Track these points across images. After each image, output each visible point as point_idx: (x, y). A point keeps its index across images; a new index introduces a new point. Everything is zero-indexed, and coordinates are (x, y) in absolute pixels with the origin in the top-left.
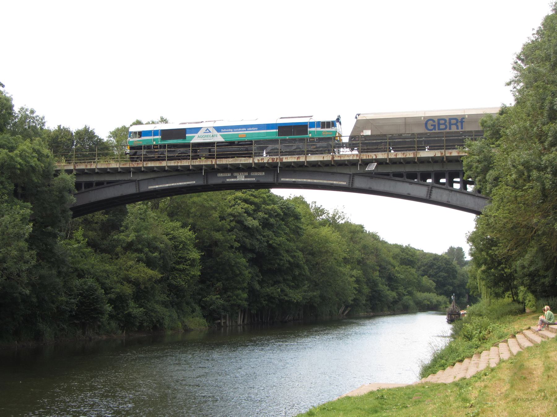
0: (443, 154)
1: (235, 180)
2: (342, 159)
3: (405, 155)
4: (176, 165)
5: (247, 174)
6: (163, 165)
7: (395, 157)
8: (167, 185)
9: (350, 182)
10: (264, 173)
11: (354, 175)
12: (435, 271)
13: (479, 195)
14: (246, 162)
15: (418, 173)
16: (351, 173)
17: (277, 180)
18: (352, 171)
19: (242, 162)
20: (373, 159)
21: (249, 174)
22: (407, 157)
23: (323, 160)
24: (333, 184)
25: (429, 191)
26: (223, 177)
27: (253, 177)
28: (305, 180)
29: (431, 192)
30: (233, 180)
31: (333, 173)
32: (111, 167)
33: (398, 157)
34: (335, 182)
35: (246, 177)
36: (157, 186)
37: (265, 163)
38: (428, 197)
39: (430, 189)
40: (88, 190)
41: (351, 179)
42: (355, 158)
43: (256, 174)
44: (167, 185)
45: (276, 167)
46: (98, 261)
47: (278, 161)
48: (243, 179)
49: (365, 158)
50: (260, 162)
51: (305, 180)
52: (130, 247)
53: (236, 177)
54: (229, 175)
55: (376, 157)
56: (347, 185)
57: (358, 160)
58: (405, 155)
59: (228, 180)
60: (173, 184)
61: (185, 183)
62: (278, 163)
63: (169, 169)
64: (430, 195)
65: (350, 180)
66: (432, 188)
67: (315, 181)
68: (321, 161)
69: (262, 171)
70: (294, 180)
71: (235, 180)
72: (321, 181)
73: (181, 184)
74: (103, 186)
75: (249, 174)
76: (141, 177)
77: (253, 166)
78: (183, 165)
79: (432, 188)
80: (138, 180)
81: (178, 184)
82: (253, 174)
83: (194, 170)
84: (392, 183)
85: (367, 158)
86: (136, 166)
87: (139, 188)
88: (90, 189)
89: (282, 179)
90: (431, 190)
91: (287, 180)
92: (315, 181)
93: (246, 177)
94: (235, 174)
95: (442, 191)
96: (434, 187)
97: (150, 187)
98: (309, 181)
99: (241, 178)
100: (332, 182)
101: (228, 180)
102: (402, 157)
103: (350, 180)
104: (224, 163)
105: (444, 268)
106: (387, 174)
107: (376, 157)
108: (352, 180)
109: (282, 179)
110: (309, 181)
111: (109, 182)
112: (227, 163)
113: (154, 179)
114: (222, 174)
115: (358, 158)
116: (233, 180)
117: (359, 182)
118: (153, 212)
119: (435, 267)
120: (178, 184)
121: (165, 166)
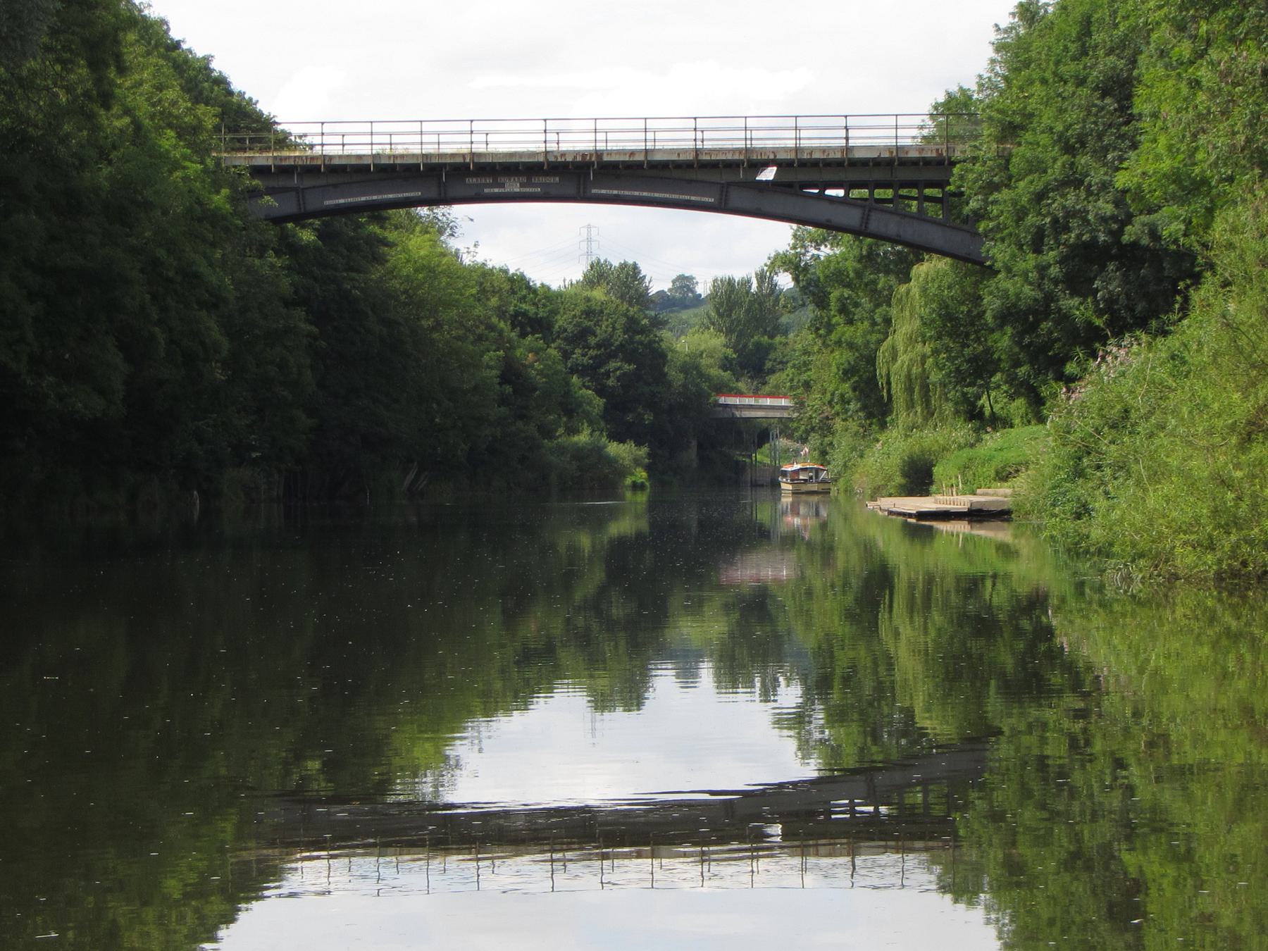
3: (826, 154)
4: (392, 162)
5: (524, 180)
8: (363, 199)
9: (721, 199)
10: (557, 179)
11: (729, 184)
12: (592, 353)
13: (965, 227)
16: (722, 182)
18: (727, 177)
19: (523, 160)
21: (529, 179)
23: (677, 159)
24: (339, 205)
25: (865, 217)
26: (477, 185)
29: (868, 219)
30: (496, 190)
31: (690, 181)
32: (256, 164)
33: (813, 157)
35: (522, 185)
37: (569, 162)
41: (724, 194)
43: (542, 180)
45: (844, 162)
47: (593, 159)
48: (518, 190)
49: (755, 158)
50: (559, 160)
52: (1042, 290)
53: (502, 185)
55: (775, 156)
57: (743, 162)
58: (826, 154)
60: (375, 197)
61: (400, 195)
62: (593, 162)
64: (867, 223)
66: (870, 211)
69: (554, 175)
71: (502, 190)
73: (391, 196)
75: (529, 179)
76: (308, 182)
78: (404, 162)
79: (870, 211)
80: (303, 189)
82: (535, 180)
85: (759, 158)
86: (308, 163)
89: (594, 191)
90: (869, 215)
94: (501, 180)
97: (327, 203)
104: (488, 161)
105: (621, 345)
108: (726, 196)
109: (594, 191)
113: (335, 186)
114: (474, 180)
115: (742, 157)
116: (496, 190)
117: (736, 197)
118: (1032, 225)
119: (592, 341)
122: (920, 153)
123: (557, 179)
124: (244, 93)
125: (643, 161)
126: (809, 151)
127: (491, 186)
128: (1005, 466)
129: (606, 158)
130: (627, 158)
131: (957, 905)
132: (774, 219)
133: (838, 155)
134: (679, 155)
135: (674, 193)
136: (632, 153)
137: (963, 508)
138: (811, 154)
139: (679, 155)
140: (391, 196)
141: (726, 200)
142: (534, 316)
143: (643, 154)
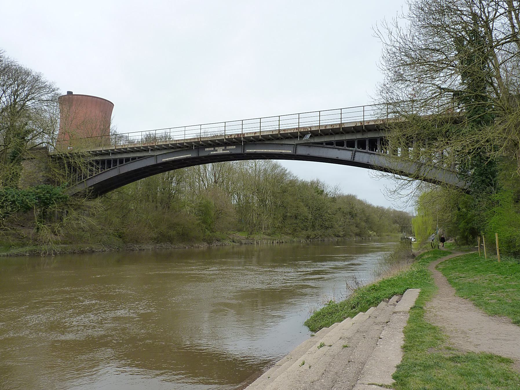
0: (363, 124)
2: (286, 132)
5: (224, 148)
6: (168, 143)
7: (325, 128)
8: (174, 158)
10: (235, 147)
11: (297, 145)
14: (220, 138)
15: (344, 141)
17: (243, 151)
18: (298, 141)
19: (217, 139)
20: (308, 131)
22: (334, 127)
24: (166, 161)
27: (228, 150)
28: (262, 151)
30: (215, 152)
34: (283, 151)
35: (223, 150)
36: (167, 159)
38: (352, 160)
39: (354, 153)
40: (126, 163)
41: (295, 148)
42: (295, 131)
43: (230, 147)
44: (174, 158)
46: (59, 188)
50: (229, 138)
51: (262, 151)
53: (217, 151)
54: (212, 149)
55: (311, 129)
56: (292, 152)
59: (211, 153)
61: (185, 156)
63: (227, 141)
64: (354, 157)
65: (294, 149)
66: (355, 152)
67: (270, 151)
68: (271, 135)
70: (255, 151)
72: (273, 151)
74: (136, 160)
77: (225, 141)
80: (156, 155)
81: (180, 157)
82: (228, 148)
83: (187, 147)
84: (326, 150)
87: (156, 161)
88: (128, 162)
89: (247, 151)
90: (355, 154)
91: (251, 151)
92: (270, 151)
93: (223, 150)
94: (216, 148)
95: (363, 154)
96: (357, 151)
97: (163, 160)
98: (265, 151)
99: (220, 151)
100: (281, 151)
101: (211, 153)
102: (331, 128)
103: (294, 149)
106: (321, 143)
107: (311, 129)
108: (296, 149)
109: (247, 151)
110: (265, 151)
111: (139, 158)
112: (208, 140)
115: (297, 131)
116: (215, 152)
120: (180, 157)
121: (259, 136)
122: (375, 122)
123: (235, 147)
126: (325, 126)
127: (212, 151)
128: (500, 362)
133: (338, 127)
134: (273, 132)
136: (273, 131)
137: (309, 289)
138: (326, 127)
139: (273, 132)
140: (182, 157)
141: (295, 151)
143: (318, 127)
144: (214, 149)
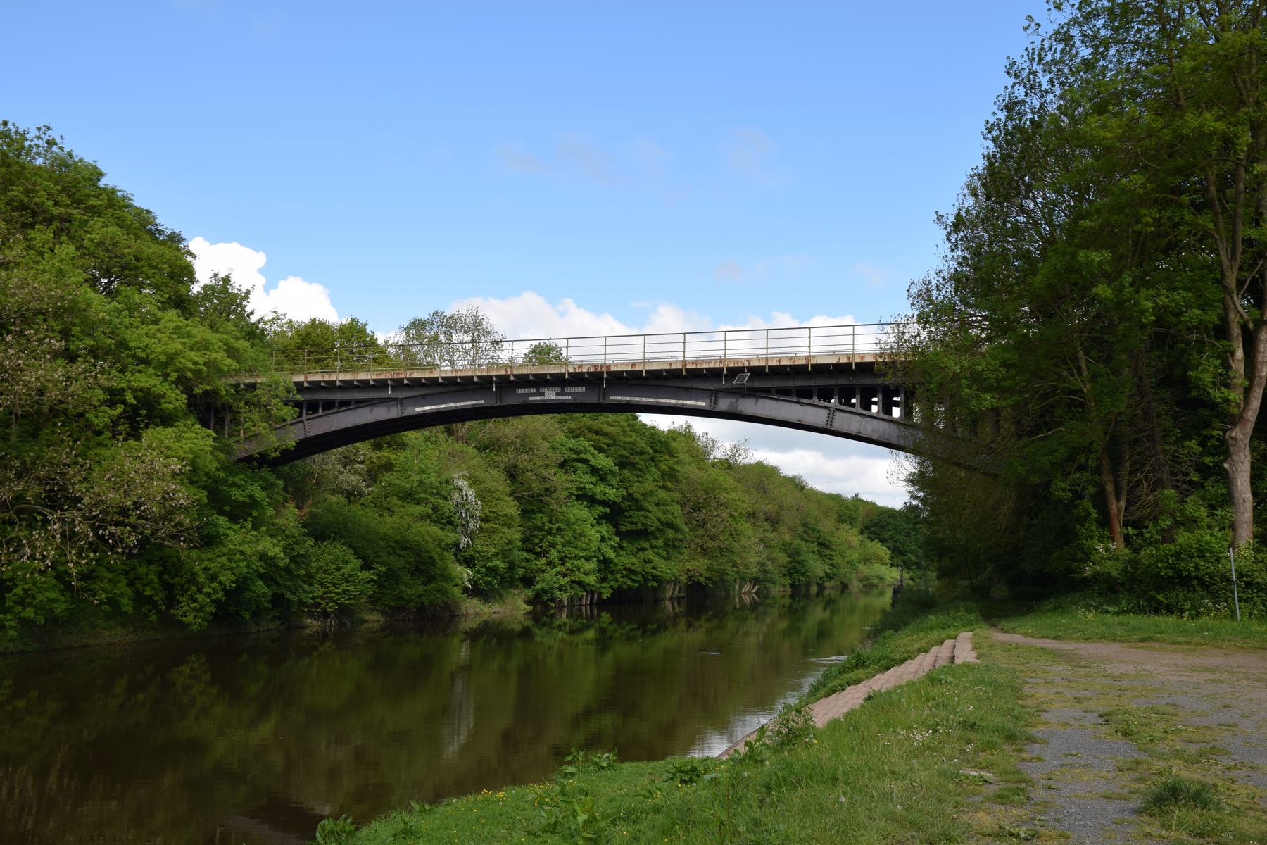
1: (542, 398)
5: (559, 389)
10: (584, 388)
21: (563, 389)
25: (831, 416)
27: (568, 394)
30: (538, 398)
31: (687, 389)
43: (573, 389)
48: (554, 398)
53: (543, 394)
54: (534, 391)
59: (531, 399)
70: (628, 398)
71: (542, 398)
75: (563, 389)
82: (568, 390)
89: (611, 398)
94: (542, 390)
101: (531, 399)
109: (611, 398)
113: (423, 396)
114: (522, 390)
116: (538, 398)
123: (584, 388)
124: (101, 175)
125: (681, 370)
129: (613, 369)
130: (629, 369)
131: (103, 170)
132: (388, 420)
134: (671, 364)
135: (690, 400)
138: (779, 361)
139: (671, 364)
140: (462, 404)
142: (683, 603)
144: (538, 390)
